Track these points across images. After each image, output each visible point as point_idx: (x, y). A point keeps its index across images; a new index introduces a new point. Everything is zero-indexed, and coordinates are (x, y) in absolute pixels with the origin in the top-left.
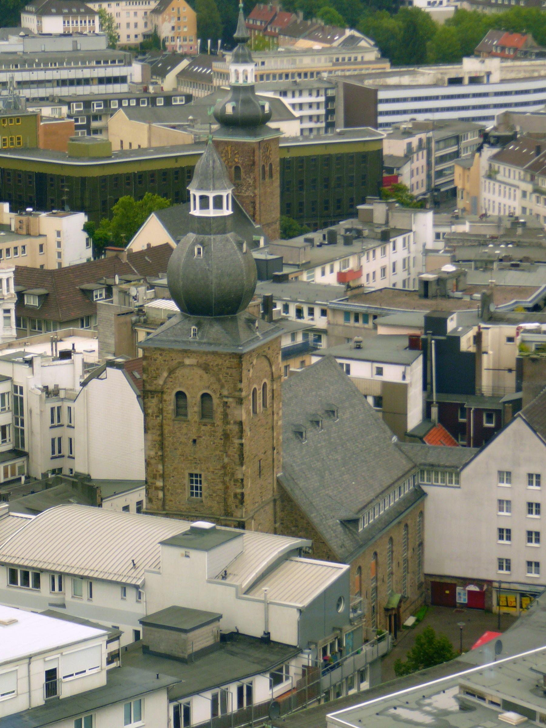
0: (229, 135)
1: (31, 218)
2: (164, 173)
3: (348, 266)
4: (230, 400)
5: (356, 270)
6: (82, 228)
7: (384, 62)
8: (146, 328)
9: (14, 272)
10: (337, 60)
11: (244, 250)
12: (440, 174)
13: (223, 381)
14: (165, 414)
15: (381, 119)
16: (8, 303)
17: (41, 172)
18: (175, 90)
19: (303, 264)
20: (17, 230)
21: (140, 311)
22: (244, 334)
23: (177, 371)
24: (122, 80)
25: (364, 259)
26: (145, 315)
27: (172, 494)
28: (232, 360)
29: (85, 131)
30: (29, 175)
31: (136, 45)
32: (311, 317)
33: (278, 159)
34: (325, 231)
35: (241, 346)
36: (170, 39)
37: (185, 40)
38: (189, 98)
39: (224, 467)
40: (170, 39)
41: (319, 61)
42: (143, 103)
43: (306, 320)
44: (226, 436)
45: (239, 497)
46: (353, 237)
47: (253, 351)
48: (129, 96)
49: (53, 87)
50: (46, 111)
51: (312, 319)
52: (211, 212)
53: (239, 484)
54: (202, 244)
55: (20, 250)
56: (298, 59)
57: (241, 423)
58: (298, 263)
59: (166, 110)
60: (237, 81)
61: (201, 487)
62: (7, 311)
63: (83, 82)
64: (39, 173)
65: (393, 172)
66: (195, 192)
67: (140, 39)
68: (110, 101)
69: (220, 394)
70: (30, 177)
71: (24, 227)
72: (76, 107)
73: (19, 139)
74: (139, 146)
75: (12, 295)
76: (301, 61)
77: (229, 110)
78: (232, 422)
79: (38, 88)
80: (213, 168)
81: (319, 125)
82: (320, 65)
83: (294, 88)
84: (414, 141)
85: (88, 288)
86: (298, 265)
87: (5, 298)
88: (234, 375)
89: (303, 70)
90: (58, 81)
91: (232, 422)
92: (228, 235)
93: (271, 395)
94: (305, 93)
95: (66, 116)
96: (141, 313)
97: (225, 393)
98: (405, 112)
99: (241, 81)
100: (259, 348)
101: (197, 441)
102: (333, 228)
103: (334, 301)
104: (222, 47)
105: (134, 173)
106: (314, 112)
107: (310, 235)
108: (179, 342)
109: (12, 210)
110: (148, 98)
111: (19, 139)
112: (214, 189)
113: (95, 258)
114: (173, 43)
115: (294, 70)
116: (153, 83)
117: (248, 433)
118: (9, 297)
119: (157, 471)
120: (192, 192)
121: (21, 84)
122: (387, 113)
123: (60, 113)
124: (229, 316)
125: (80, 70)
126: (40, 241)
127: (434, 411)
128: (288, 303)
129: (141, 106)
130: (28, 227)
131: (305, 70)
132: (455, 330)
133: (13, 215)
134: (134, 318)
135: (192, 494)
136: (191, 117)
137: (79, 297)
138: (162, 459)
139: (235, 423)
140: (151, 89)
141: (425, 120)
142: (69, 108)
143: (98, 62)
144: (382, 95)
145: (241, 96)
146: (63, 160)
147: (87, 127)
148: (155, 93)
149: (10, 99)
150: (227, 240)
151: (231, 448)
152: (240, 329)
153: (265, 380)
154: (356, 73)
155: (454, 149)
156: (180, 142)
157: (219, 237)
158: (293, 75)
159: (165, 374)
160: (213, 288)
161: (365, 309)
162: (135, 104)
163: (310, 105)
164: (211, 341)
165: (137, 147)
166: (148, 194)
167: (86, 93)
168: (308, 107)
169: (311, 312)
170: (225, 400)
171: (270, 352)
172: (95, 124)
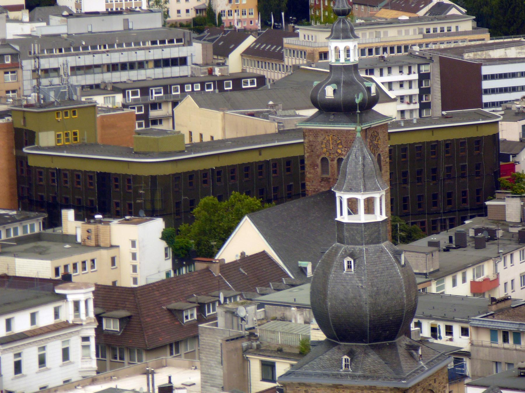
0: (330, 123)
1: (101, 226)
2: (246, 168)
3: (483, 275)
5: (492, 278)
6: (160, 236)
7: (483, 33)
8: (259, 355)
9: (94, 292)
10: (428, 31)
11: (403, 263)
15: (486, 99)
16: (87, 329)
17: (103, 171)
18: (244, 71)
19: (431, 273)
20: (84, 241)
21: (252, 335)
22: (406, 365)
24: (183, 61)
25: (501, 265)
26: (258, 339)
29: (143, 121)
30: (89, 175)
31: (187, 21)
32: (449, 337)
33: (387, 149)
34: (452, 232)
35: (404, 379)
36: (226, 13)
37: (244, 13)
38: (261, 80)
40: (226, 13)
41: (407, 32)
42: (209, 87)
43: (444, 340)
46: (486, 239)
47: (418, 384)
48: (192, 80)
49: (102, 73)
50: (100, 100)
51: (451, 340)
52: (362, 218)
54: (352, 255)
55: (88, 264)
56: (382, 31)
58: (425, 272)
59: (238, 95)
60: (337, 60)
62: (86, 339)
63: (137, 65)
64: (101, 173)
65: (509, 161)
66: (343, 197)
67: (192, 15)
68: (171, 86)
70: (91, 177)
71: (93, 237)
72: (133, 95)
73: (75, 134)
74: (212, 138)
75: (90, 318)
76: (386, 33)
77: (329, 92)
79: (85, 74)
80: (364, 165)
81: (412, 107)
82: (407, 38)
83: (381, 65)
85: (177, 308)
86: (425, 274)
87: (84, 323)
89: (388, 45)
90: (108, 65)
92: (383, 245)
94: (395, 70)
95: (121, 105)
96: (252, 338)
98: (514, 89)
99: (342, 60)
100: (425, 380)
102: (459, 228)
103: (477, 318)
104: (288, 21)
105: (212, 169)
106: (406, 91)
107: (434, 238)
108: (328, 375)
109: (77, 218)
110: (214, 82)
111: (75, 134)
112: (365, 190)
113: (175, 272)
114: (230, 18)
115: (378, 45)
116: (218, 65)
118: (88, 321)
120: (338, 194)
121: (76, 70)
122: (493, 91)
123: (114, 103)
124: (387, 343)
125: (134, 52)
126: (112, 252)
128: (421, 320)
129: (207, 90)
130: (97, 236)
131: (391, 44)
133: (79, 223)
134: (245, 344)
136: (271, 103)
137: (167, 319)
140: (217, 71)
142: (124, 96)
143: (154, 43)
144: (486, 70)
145: (343, 77)
146: (129, 157)
147: (145, 117)
148: (222, 76)
149: (65, 88)
150: (382, 251)
152: (402, 358)
154: (452, 45)
156: (261, 132)
157: (372, 247)
158: (377, 49)
160: (368, 309)
161: (517, 326)
162: (199, 89)
163: (401, 84)
164: (367, 374)
165: (209, 139)
166: (235, 195)
167: (140, 78)
168: (399, 86)
169: (449, 331)
171: (436, 385)
172: (154, 114)
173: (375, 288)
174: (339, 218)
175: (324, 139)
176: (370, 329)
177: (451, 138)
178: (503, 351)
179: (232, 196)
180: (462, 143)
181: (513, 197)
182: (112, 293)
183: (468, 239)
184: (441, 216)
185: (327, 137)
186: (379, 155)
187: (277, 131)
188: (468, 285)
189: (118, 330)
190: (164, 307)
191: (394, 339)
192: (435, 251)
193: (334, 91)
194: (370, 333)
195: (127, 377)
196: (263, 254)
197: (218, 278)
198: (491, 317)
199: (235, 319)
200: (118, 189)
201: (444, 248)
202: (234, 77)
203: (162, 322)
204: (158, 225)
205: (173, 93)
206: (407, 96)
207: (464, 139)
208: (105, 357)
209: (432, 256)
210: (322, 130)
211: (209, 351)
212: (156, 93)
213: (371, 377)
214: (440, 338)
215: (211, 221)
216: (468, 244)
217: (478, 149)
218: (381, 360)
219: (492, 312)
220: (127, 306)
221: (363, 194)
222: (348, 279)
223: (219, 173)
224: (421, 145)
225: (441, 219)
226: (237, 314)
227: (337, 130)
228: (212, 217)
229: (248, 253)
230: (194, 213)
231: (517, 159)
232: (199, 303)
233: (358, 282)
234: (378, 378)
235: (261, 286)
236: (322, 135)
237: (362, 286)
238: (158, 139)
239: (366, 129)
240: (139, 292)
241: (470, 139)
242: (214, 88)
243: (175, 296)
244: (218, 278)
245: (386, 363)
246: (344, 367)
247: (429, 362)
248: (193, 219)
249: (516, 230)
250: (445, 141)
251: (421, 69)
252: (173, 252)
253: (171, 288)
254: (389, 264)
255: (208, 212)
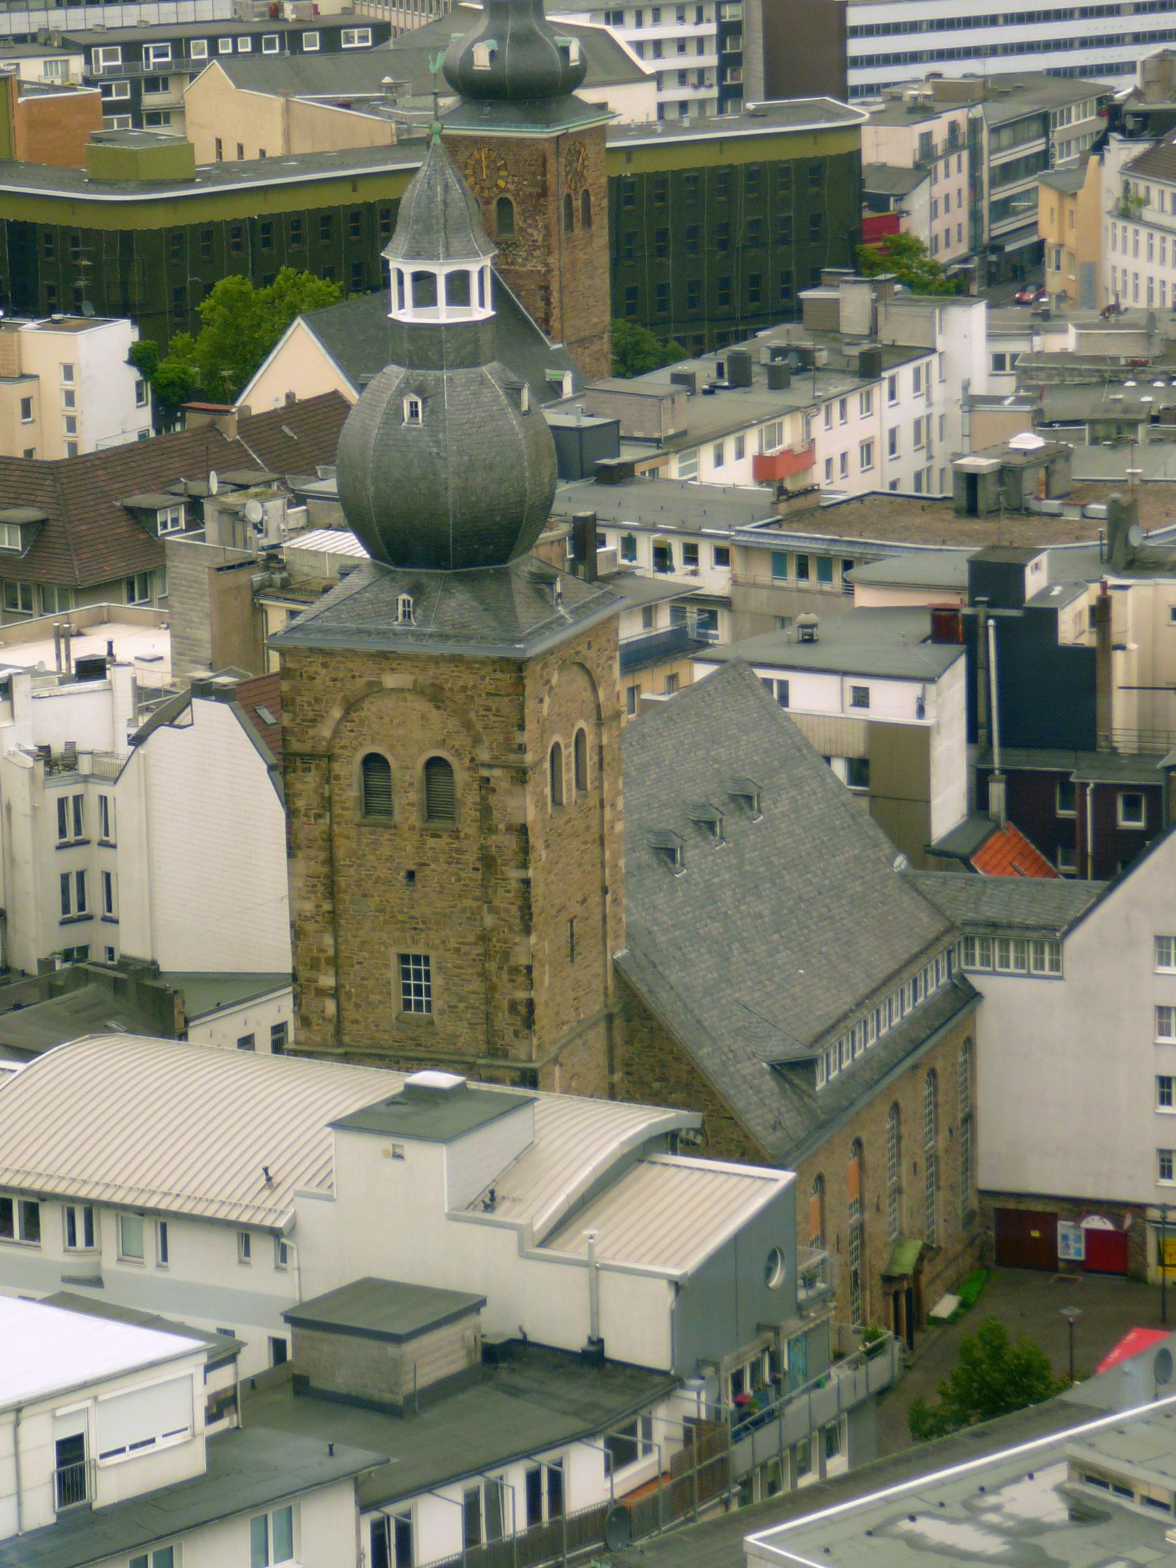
0: (482, 122)
2: (325, 218)
3: (780, 442)
4: (497, 773)
5: (798, 450)
6: (126, 357)
12: (1002, 209)
13: (479, 727)
14: (337, 810)
15: (856, 77)
19: (669, 438)
21: (273, 559)
22: (527, 614)
23: (366, 705)
25: (818, 422)
26: (284, 568)
27: (357, 1006)
28: (499, 675)
32: (692, 568)
33: (604, 180)
34: (723, 355)
35: (520, 641)
39: (484, 938)
42: (270, 45)
44: (488, 862)
45: (523, 1010)
46: (791, 368)
50: (32, 69)
51: (694, 573)
52: (443, 314)
53: (521, 979)
54: (419, 391)
57: (523, 830)
58: (656, 435)
59: (324, 61)
61: (428, 988)
65: (888, 209)
68: (188, 40)
69: (472, 760)
74: (263, 153)
78: (502, 826)
81: (703, 93)
84: (939, 128)
85: (144, 505)
86: (658, 441)
88: (505, 711)
91: (502, 826)
92: (484, 369)
93: (596, 758)
94: (669, 16)
96: (272, 565)
97: (484, 755)
98: (914, 57)
100: (567, 643)
101: (418, 876)
103: (746, 528)
105: (252, 220)
106: (690, 61)
107: (684, 367)
108: (369, 633)
110: (281, 34)
112: (448, 255)
113: (158, 432)
117: (540, 853)
119: (321, 950)
122: (870, 61)
123: (66, 75)
124: (491, 568)
126: (21, 390)
127: (997, 791)
132: (1044, 593)
134: (257, 577)
135: (407, 1005)
136: (387, 80)
137: (123, 527)
138: (333, 920)
139: (509, 829)
141: (965, 76)
142: (88, 61)
147: (133, 106)
148: (297, 21)
150: (483, 381)
151: (501, 891)
152: (518, 599)
153: (581, 724)
155: (1038, 146)
157: (461, 374)
159: (337, 713)
160: (451, 500)
163: (681, 45)
164: (448, 630)
165: (256, 156)
166: (286, 271)
167: (128, 22)
169: (691, 556)
170: (485, 773)
171: (592, 653)
172: (151, 100)
173: (466, 458)
174: (396, 314)
175: (470, 157)
176: (455, 541)
177: (761, 160)
178: (795, 594)
179: (280, 277)
180: (782, 170)
181: (855, 282)
182: (8, 472)
183: (755, 369)
184: (738, 325)
185: (476, 153)
186: (586, 191)
187: (395, 139)
188: (747, 464)
189: (20, 548)
190: (118, 504)
191: (505, 562)
192: (679, 392)
193: (492, 54)
194: (455, 549)
195: (25, 642)
196: (335, 395)
197: (234, 445)
198: (776, 526)
199: (239, 526)
200: (51, 259)
201: (706, 387)
202: (322, 25)
203: (113, 532)
204: (121, 334)
205: (193, 57)
206: (692, 70)
207: (788, 161)
208: (30, 608)
209: (673, 402)
210: (465, 138)
211: (186, 592)
212: (156, 56)
213: (454, 637)
214: (671, 569)
215: (237, 328)
216: (754, 380)
217: (815, 183)
218: (476, 604)
219: (779, 517)
220: (39, 499)
221: (442, 264)
222: (409, 438)
223: (266, 228)
224: (695, 174)
225: (736, 332)
226: (244, 516)
227: (497, 138)
228: (239, 321)
229: (302, 395)
230: (201, 313)
231: (905, 206)
232: (189, 496)
233: (431, 444)
234: (469, 638)
235: (327, 464)
236: (467, 148)
237: (438, 454)
238: (135, 153)
239: (558, 137)
240: (63, 470)
241: (799, 162)
242: (282, 48)
243: (141, 480)
244: (234, 445)
245: (485, 610)
246: (400, 618)
247: (577, 608)
248: (196, 326)
249: (855, 351)
250: (747, 165)
251: (723, 13)
252: (153, 392)
253: (133, 464)
254: (495, 408)
255: (231, 310)
